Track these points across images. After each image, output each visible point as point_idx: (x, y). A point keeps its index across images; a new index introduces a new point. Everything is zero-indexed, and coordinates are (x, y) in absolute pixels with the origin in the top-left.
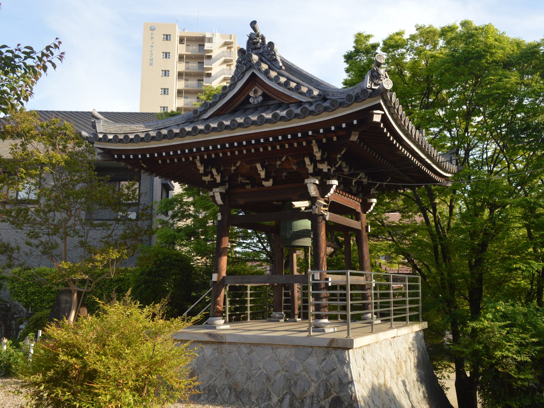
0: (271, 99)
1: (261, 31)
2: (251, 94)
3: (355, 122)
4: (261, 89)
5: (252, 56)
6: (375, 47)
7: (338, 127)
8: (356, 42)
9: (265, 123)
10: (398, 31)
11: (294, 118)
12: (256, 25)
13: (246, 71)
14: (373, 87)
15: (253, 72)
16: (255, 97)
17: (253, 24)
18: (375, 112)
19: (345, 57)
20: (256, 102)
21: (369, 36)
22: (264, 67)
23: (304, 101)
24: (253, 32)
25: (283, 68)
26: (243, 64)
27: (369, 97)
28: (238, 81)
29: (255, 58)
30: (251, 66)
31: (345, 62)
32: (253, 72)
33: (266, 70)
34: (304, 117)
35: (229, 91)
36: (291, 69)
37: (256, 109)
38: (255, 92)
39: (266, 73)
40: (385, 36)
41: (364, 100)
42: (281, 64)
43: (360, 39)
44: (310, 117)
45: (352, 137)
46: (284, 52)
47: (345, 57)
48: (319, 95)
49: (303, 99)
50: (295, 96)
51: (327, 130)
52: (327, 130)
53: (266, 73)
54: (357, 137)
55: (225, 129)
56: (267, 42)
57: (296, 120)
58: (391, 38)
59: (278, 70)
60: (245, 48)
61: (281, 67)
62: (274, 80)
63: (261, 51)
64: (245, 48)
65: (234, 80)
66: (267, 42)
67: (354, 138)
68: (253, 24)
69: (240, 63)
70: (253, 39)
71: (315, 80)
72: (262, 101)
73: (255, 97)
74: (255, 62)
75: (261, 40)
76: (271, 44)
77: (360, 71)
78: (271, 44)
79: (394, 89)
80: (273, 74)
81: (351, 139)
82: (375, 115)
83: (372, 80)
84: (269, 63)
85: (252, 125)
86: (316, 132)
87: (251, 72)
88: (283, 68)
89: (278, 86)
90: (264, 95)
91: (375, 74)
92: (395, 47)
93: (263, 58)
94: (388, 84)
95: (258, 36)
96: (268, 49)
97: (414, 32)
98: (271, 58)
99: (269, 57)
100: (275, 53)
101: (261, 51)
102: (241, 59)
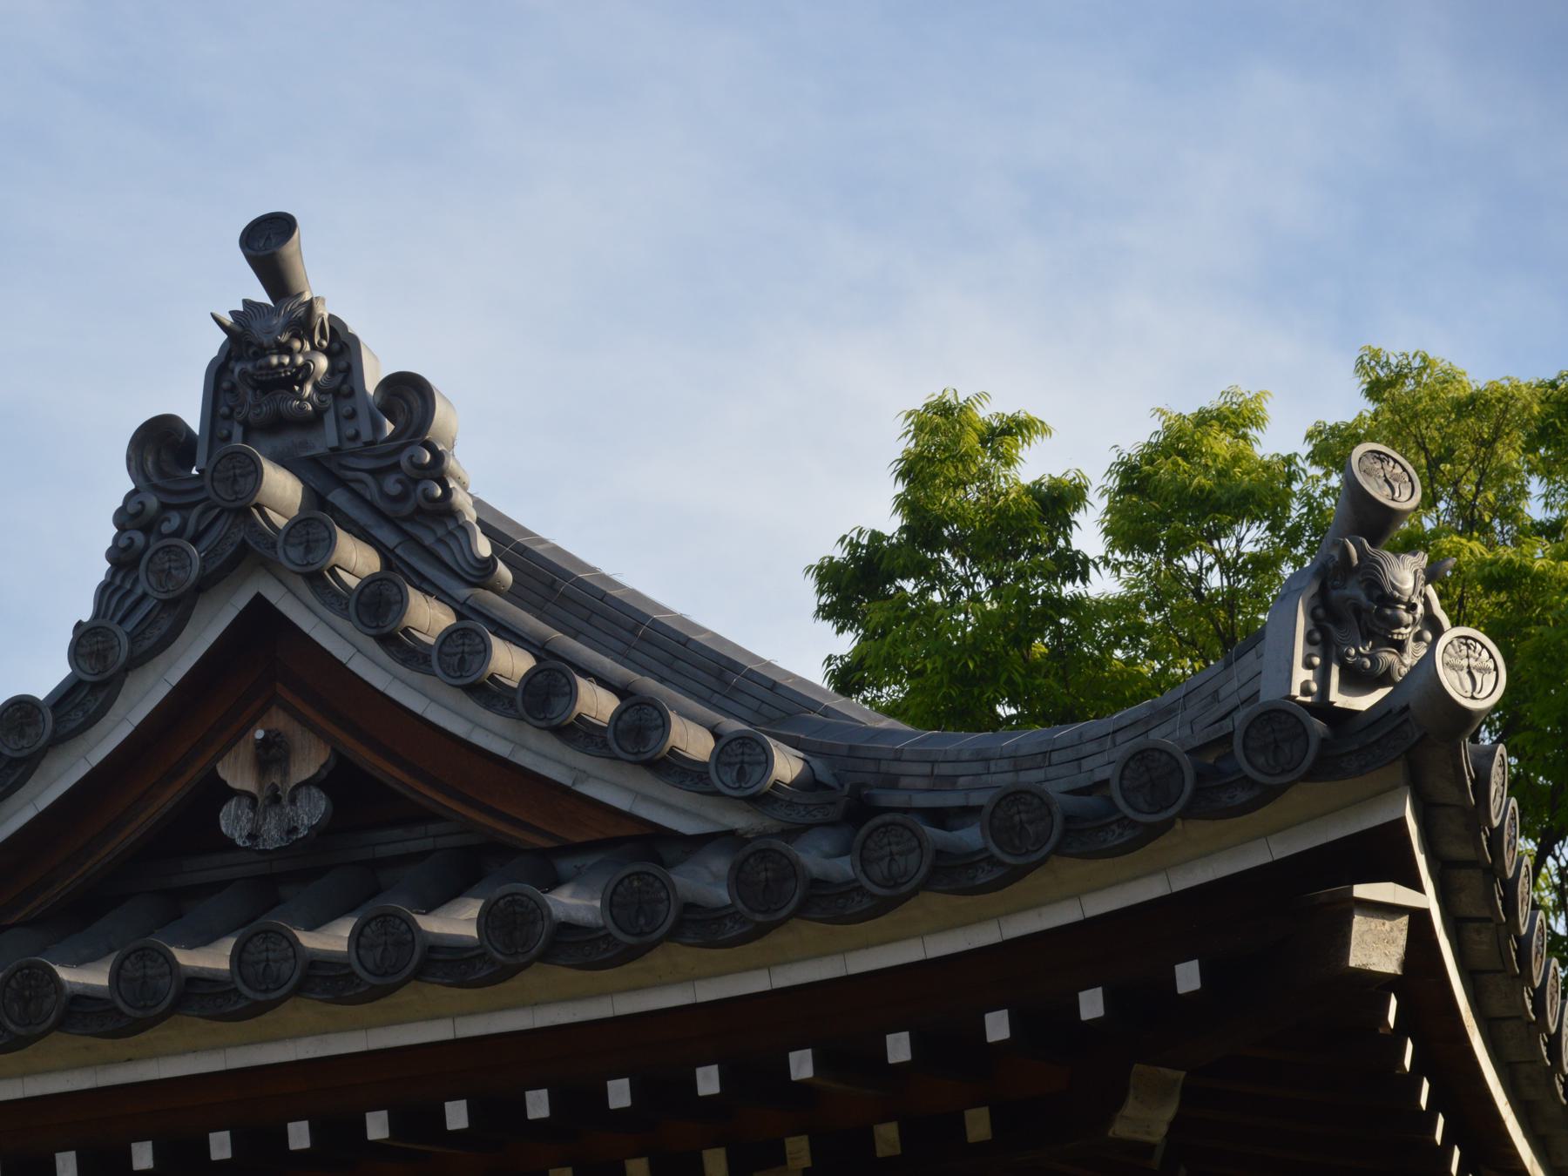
0: (409, 809)
1: (328, 280)
2: (238, 774)
3: (1188, 977)
4: (320, 734)
5: (258, 473)
6: (1058, 502)
7: (1045, 1022)
8: (914, 470)
9: (420, 974)
10: (1210, 400)
11: (673, 935)
12: (289, 249)
13: (204, 586)
14: (1338, 698)
15: (259, 602)
16: (269, 792)
17: (268, 240)
18: (1361, 891)
19: (829, 575)
20: (272, 836)
21: (1017, 428)
22: (356, 559)
23: (688, 827)
24: (261, 296)
25: (504, 572)
26: (178, 533)
27: (1311, 776)
28: (137, 661)
29: (282, 488)
30: (243, 550)
31: (826, 612)
32: (259, 602)
33: (370, 582)
34: (761, 931)
35: (60, 739)
36: (557, 590)
37: (269, 890)
38: (271, 756)
39: (376, 607)
40: (1136, 433)
41: (1270, 795)
42: (484, 547)
43: (945, 448)
44: (808, 931)
45: (1131, 1108)
46: (495, 465)
47: (829, 575)
48: (807, 783)
49: (678, 813)
50: (613, 788)
51: (951, 1044)
52: (951, 1044)
53: (376, 607)
54: (1169, 1112)
55: (61, 1025)
56: (371, 380)
57: (683, 955)
58: (1179, 442)
59: (463, 592)
60: (193, 419)
61: (488, 565)
62: (410, 658)
63: (328, 437)
64: (193, 419)
65: (101, 656)
66: (371, 380)
67: (1146, 1119)
68: (268, 240)
69: (149, 528)
70: (263, 352)
71: (752, 676)
72: (322, 832)
73: (269, 792)
74: (280, 522)
75: (322, 363)
76: (409, 393)
77: (964, 680)
78: (409, 393)
79: (1511, 716)
80: (428, 617)
81: (1120, 1129)
82: (1359, 923)
83: (1324, 642)
84: (389, 538)
85: (300, 990)
86: (851, 1057)
87: (241, 601)
88: (504, 572)
89: (470, 706)
90: (339, 780)
91: (1355, 591)
92: (1218, 507)
93: (338, 497)
94: (1473, 674)
95: (303, 323)
96: (377, 427)
97: (1347, 404)
98: (402, 498)
99: (392, 486)
100: (438, 457)
101: (328, 437)
102: (152, 502)
